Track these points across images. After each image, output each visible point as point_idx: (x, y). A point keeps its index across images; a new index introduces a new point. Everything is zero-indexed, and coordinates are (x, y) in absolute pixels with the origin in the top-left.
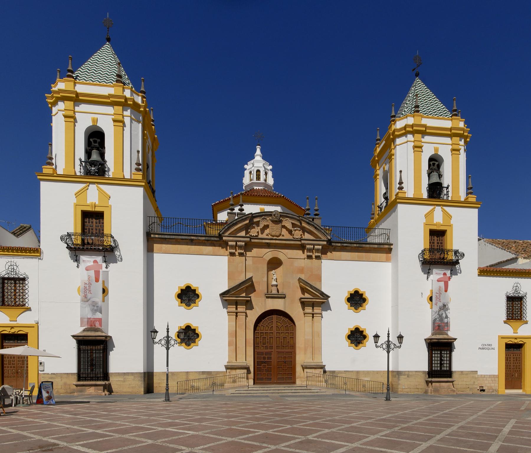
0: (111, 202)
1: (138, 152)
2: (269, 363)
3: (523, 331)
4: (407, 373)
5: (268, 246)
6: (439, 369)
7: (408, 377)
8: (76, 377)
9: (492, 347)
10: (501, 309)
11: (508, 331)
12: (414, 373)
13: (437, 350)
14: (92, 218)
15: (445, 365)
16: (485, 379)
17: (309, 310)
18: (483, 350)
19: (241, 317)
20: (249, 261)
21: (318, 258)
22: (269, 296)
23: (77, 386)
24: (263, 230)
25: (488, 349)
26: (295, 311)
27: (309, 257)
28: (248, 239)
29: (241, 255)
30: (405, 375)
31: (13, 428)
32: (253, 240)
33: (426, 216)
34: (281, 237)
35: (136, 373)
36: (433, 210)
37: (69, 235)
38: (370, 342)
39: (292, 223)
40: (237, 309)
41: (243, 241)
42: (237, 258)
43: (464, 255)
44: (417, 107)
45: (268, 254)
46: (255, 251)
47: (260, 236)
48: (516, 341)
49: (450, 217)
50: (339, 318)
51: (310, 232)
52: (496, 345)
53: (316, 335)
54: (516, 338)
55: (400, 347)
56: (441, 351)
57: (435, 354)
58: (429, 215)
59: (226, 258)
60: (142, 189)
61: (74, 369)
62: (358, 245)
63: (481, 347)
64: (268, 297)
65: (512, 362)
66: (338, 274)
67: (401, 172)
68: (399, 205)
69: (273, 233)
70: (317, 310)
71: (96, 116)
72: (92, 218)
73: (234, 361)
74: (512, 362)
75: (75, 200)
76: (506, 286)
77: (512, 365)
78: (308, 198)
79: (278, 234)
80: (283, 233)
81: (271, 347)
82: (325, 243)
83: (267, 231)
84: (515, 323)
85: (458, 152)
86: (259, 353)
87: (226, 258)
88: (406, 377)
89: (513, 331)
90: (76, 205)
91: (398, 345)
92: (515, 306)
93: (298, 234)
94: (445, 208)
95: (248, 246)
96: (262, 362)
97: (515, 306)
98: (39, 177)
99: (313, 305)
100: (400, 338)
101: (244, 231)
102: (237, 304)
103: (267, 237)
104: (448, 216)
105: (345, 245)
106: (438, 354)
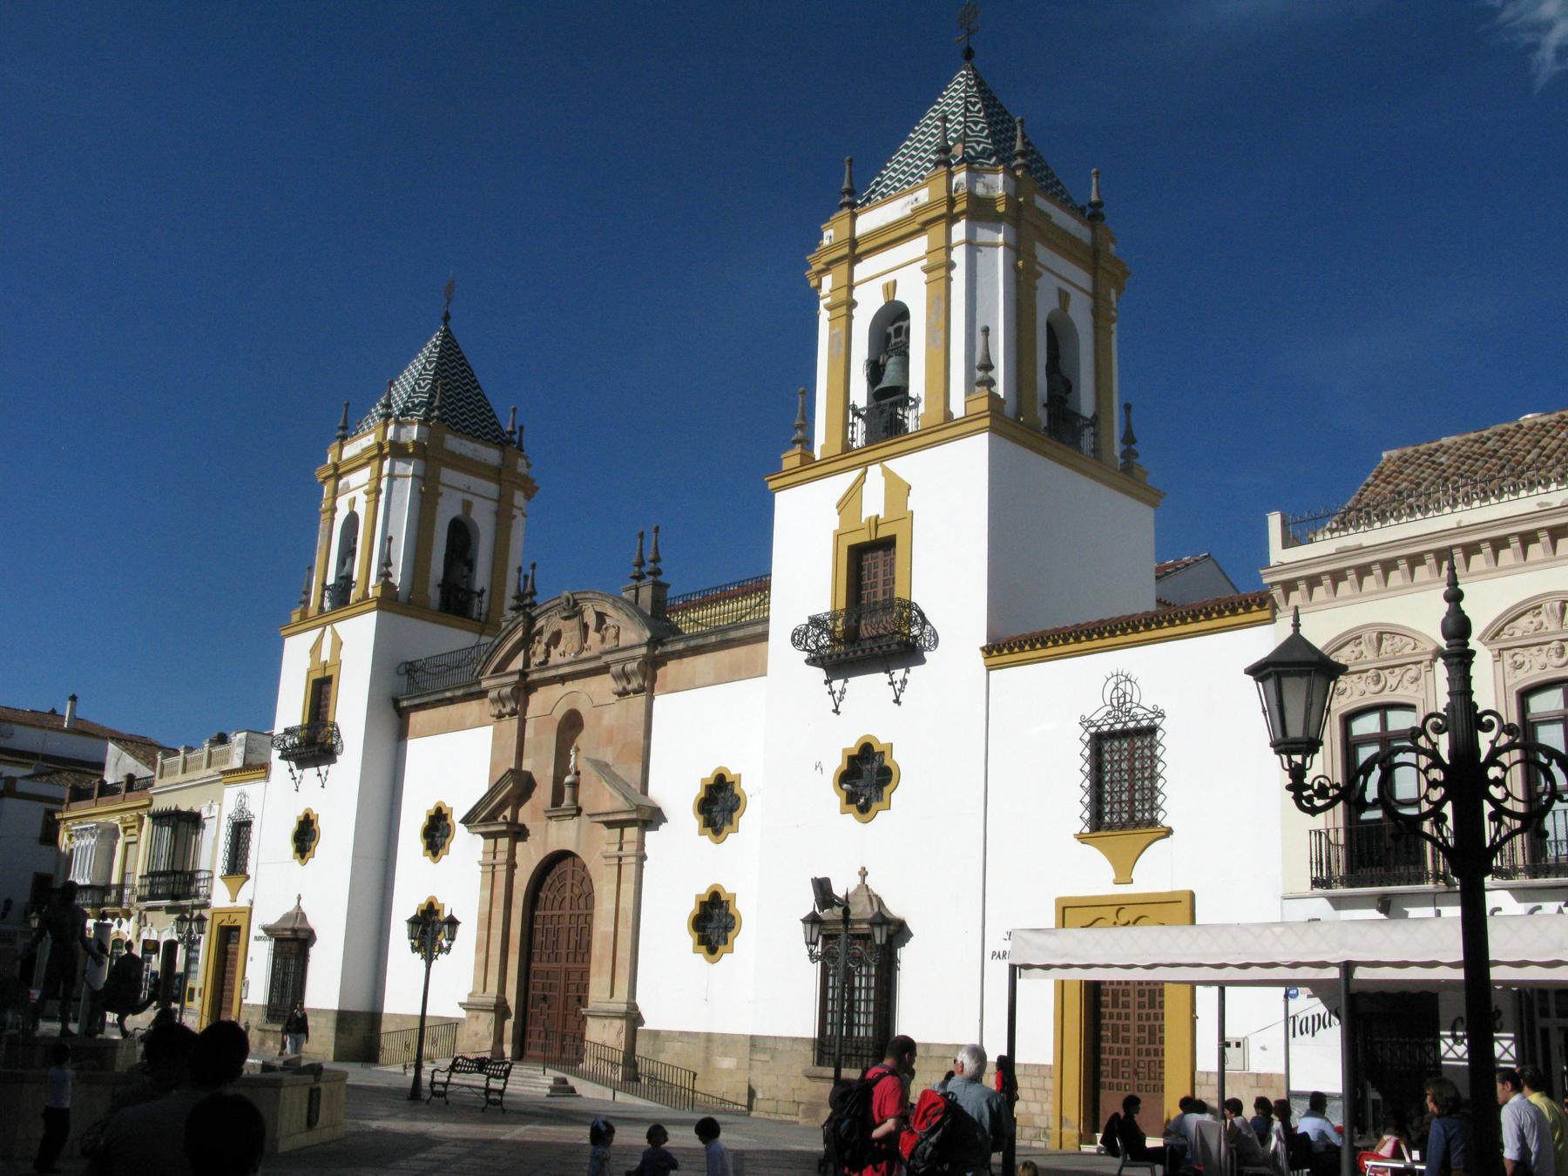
14: (870, 560)
30: (764, 1050)
33: (842, 505)
40: (621, 849)
50: (679, 864)
61: (808, 1027)
68: (779, 496)
72: (870, 560)
104: (898, 490)
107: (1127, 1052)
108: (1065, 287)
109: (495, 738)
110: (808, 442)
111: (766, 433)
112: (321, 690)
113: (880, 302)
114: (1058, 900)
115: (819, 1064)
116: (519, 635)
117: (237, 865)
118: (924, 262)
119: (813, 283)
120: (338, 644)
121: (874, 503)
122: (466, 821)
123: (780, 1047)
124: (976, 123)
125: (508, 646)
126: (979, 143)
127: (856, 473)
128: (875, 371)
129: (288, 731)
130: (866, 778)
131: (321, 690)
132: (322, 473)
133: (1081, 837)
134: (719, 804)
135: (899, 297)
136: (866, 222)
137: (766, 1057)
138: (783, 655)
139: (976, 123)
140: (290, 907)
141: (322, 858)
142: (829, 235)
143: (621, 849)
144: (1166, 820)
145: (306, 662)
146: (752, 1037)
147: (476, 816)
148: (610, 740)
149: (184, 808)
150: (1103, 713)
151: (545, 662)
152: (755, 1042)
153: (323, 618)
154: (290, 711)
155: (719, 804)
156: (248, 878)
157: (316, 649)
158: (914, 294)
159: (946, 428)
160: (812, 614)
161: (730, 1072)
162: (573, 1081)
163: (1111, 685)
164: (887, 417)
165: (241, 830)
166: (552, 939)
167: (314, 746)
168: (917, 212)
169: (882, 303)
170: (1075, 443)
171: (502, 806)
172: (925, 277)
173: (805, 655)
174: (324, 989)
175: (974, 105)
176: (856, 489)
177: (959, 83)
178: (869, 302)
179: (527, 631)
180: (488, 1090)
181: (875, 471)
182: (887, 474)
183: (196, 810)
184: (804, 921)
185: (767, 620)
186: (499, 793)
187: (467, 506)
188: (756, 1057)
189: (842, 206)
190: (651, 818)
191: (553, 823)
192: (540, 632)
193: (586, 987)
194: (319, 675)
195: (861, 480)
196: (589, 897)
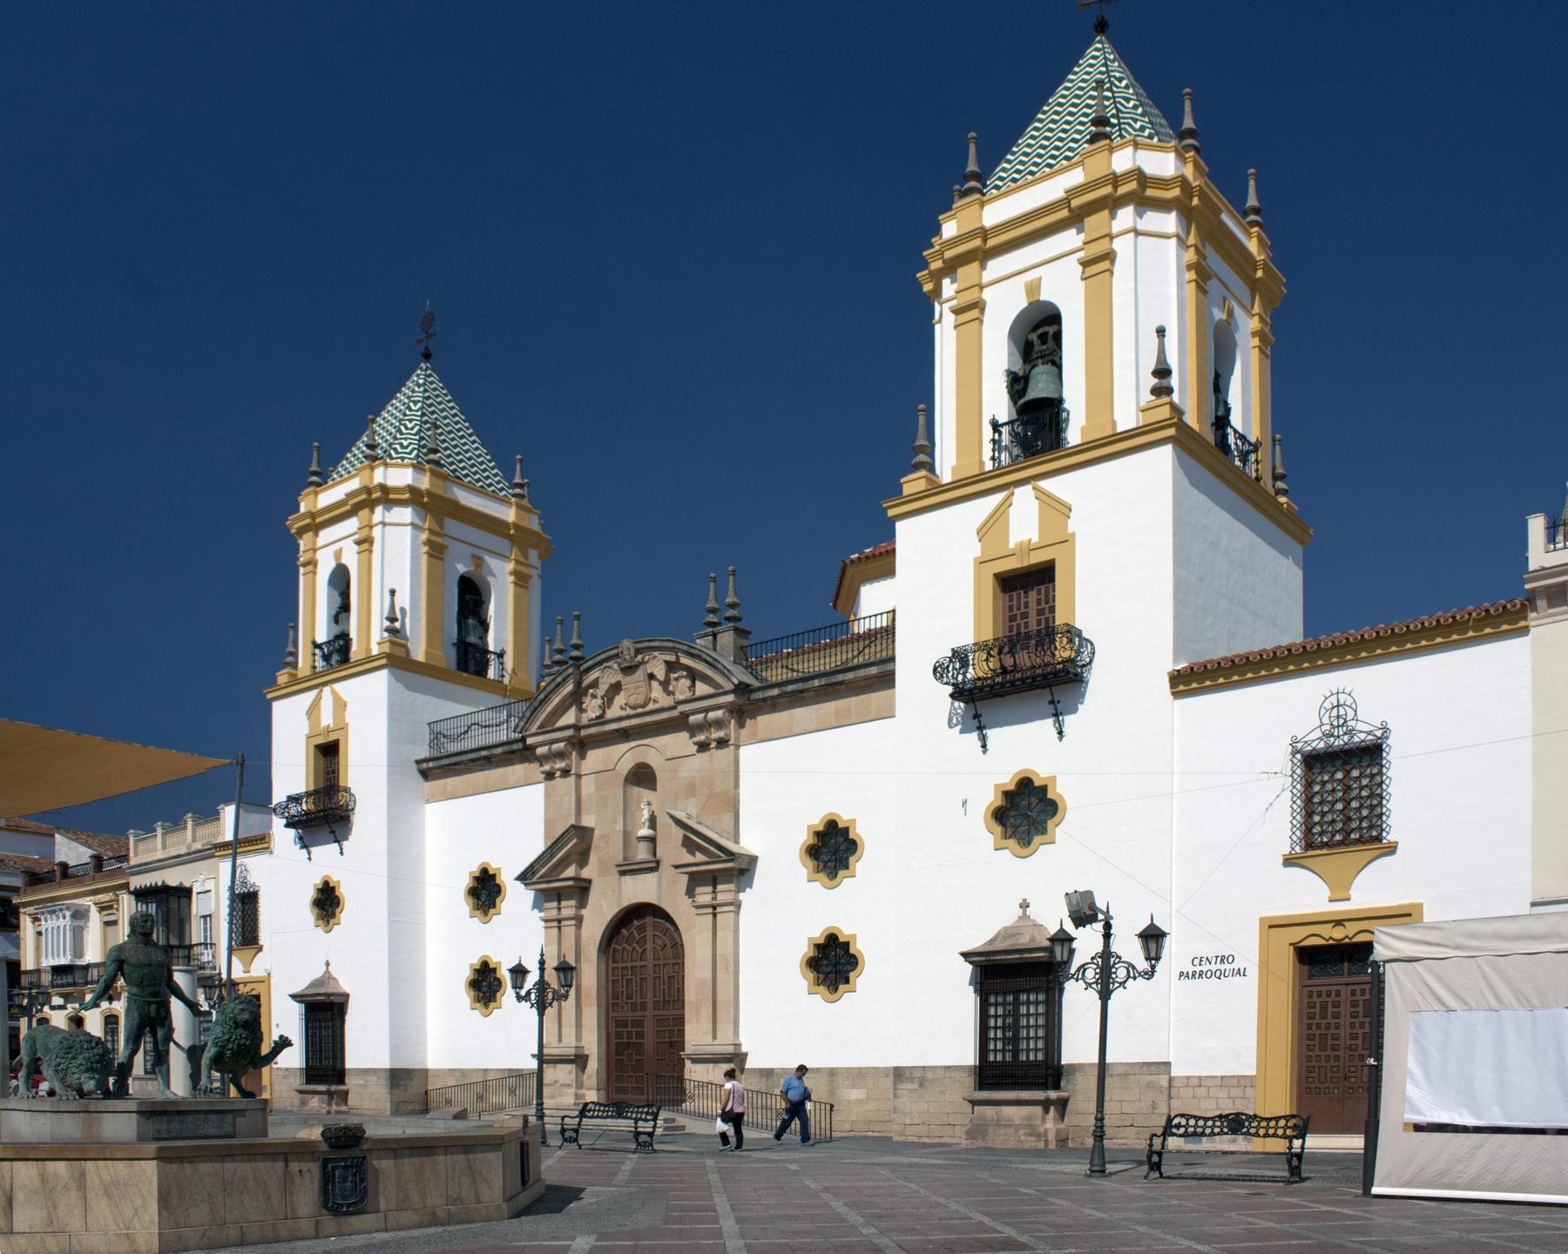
0: (1072, 526)
1: (1161, 332)
2: (638, 1048)
3: (1374, 886)
4: (918, 1074)
5: (625, 735)
6: (1009, 1057)
7: (921, 1085)
8: (970, 1081)
9: (1235, 966)
10: (1276, 814)
11: (1308, 896)
12: (941, 1073)
13: (1037, 990)
14: (1027, 586)
15: (1000, 1045)
16: (1202, 1091)
17: (704, 895)
18: (1197, 982)
19: (569, 930)
20: (588, 786)
21: (722, 743)
22: (629, 869)
23: (974, 1103)
24: (609, 698)
25: (1220, 975)
26: (679, 907)
27: (703, 747)
28: (570, 732)
29: (566, 773)
30: (912, 1080)
31: (1008, 1224)
32: (583, 733)
33: (983, 532)
34: (651, 706)
35: (956, 1067)
36: (1006, 504)
37: (960, 656)
38: (508, 995)
39: (667, 662)
40: (714, 898)
41: (718, 707)
42: (559, 782)
43: (935, 669)
44: (1101, 121)
45: (623, 756)
46: (595, 758)
47: (610, 714)
48: (1338, 934)
49: (1065, 509)
50: (781, 912)
51: (706, 679)
52: (1248, 953)
53: (725, 966)
54: (1339, 923)
55: (1149, 974)
56: (1016, 993)
57: (1028, 1003)
58: (992, 528)
59: (538, 790)
60: (1167, 450)
61: (968, 1055)
62: (823, 681)
63: (1191, 969)
64: (623, 873)
65: (1345, 1019)
66: (783, 779)
67: (393, 592)
68: (900, 526)
69: (632, 701)
70: (725, 892)
71: (336, 546)
72: (1027, 586)
73: (708, 1039)
74: (1345, 1019)
75: (976, 550)
76: (1296, 709)
77: (1344, 1033)
78: (578, 618)
79: (641, 701)
80: (653, 695)
81: (644, 1007)
82: (730, 698)
83: (620, 700)
84: (1342, 860)
85: (975, 313)
86: (620, 1023)
87: (538, 790)
88: (915, 1086)
89: (1327, 893)
90: (981, 562)
91: (1142, 965)
92: (1341, 793)
93: (682, 687)
94: (1043, 484)
95: (582, 745)
96: (628, 1045)
97: (1341, 793)
98: (891, 513)
99: (714, 879)
100: (1152, 938)
101: (574, 709)
102: (558, 895)
103: (624, 713)
104: (1056, 510)
105: (790, 688)
106: (1037, 1003)
107: (1337, 1058)
108: (478, 552)
109: (547, 796)
110: (295, 665)
111: (871, 458)
112: (328, 752)
113: (333, 565)
114: (1262, 920)
115: (981, 1089)
116: (569, 687)
117: (246, 933)
118: (1081, 254)
119: (928, 287)
120: (340, 705)
121: (327, 719)
122: (523, 877)
123: (930, 1075)
124: (1128, 100)
125: (556, 700)
126: (1136, 121)
127: (998, 497)
128: (1017, 384)
129: (291, 799)
130: (327, 902)
131: (328, 752)
132: (294, 523)
133: (1289, 861)
134: (832, 849)
135: (343, 561)
136: (995, 213)
137: (915, 1086)
138: (920, 694)
139: (1128, 100)
140: (319, 972)
141: (398, 919)
142: (949, 229)
143: (714, 898)
144: (1390, 837)
145: (304, 728)
146: (896, 1069)
147: (534, 874)
148: (692, 790)
149: (173, 882)
150: (1318, 733)
151: (601, 716)
152: (899, 1074)
153: (316, 681)
154: (290, 774)
155: (832, 849)
156: (260, 949)
157: (313, 711)
158: (1065, 289)
159: (1111, 446)
160: (955, 646)
161: (859, 1102)
162: (681, 1120)
163: (1334, 700)
164: (1037, 427)
165: (245, 904)
166: (640, 991)
167: (325, 816)
168: (350, 495)
169: (1023, 303)
170: (481, 671)
171: (564, 863)
172: (356, 548)
173: (950, 689)
174: (366, 1048)
175: (1120, 80)
176: (1001, 513)
177: (1095, 58)
178: (325, 567)
179: (578, 683)
180: (637, 1134)
181: (327, 690)
182: (334, 693)
183: (187, 885)
184: (347, 996)
185: (892, 659)
186: (560, 849)
187: (478, 561)
188: (900, 1086)
189: (312, 484)
190: (741, 870)
191: (628, 879)
192: (595, 684)
193: (682, 1033)
194: (321, 740)
195: (318, 698)
196: (677, 949)
